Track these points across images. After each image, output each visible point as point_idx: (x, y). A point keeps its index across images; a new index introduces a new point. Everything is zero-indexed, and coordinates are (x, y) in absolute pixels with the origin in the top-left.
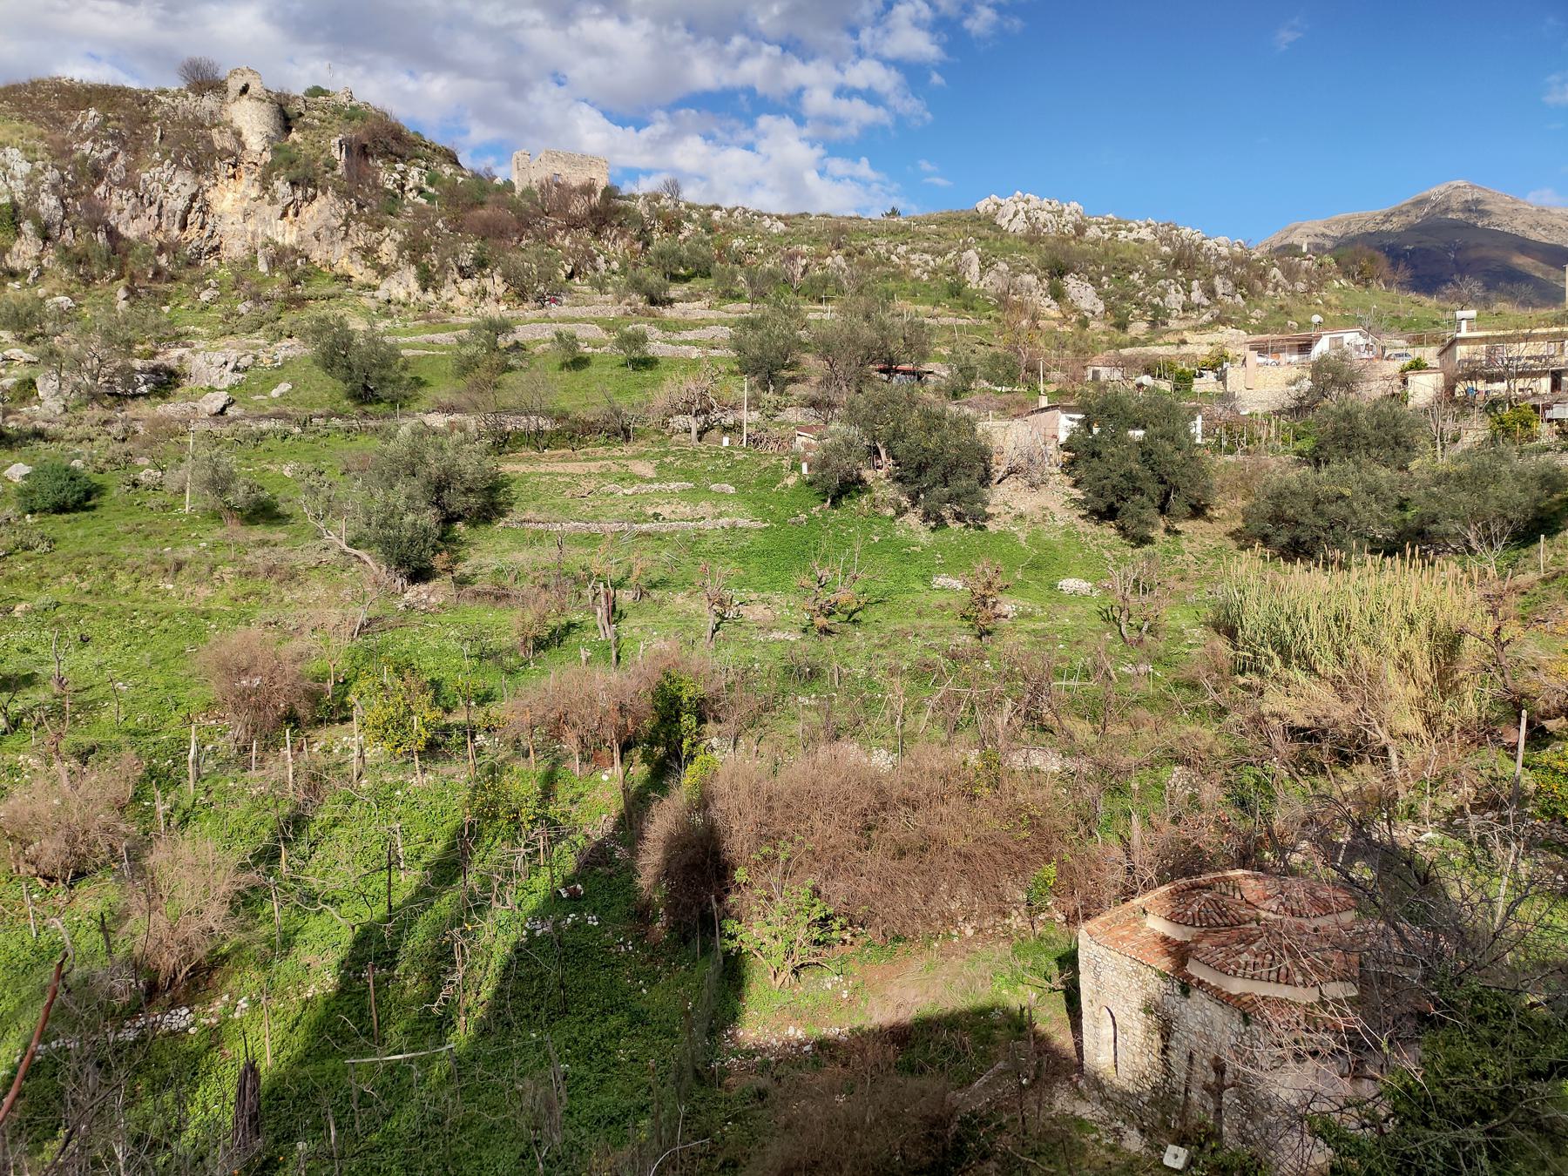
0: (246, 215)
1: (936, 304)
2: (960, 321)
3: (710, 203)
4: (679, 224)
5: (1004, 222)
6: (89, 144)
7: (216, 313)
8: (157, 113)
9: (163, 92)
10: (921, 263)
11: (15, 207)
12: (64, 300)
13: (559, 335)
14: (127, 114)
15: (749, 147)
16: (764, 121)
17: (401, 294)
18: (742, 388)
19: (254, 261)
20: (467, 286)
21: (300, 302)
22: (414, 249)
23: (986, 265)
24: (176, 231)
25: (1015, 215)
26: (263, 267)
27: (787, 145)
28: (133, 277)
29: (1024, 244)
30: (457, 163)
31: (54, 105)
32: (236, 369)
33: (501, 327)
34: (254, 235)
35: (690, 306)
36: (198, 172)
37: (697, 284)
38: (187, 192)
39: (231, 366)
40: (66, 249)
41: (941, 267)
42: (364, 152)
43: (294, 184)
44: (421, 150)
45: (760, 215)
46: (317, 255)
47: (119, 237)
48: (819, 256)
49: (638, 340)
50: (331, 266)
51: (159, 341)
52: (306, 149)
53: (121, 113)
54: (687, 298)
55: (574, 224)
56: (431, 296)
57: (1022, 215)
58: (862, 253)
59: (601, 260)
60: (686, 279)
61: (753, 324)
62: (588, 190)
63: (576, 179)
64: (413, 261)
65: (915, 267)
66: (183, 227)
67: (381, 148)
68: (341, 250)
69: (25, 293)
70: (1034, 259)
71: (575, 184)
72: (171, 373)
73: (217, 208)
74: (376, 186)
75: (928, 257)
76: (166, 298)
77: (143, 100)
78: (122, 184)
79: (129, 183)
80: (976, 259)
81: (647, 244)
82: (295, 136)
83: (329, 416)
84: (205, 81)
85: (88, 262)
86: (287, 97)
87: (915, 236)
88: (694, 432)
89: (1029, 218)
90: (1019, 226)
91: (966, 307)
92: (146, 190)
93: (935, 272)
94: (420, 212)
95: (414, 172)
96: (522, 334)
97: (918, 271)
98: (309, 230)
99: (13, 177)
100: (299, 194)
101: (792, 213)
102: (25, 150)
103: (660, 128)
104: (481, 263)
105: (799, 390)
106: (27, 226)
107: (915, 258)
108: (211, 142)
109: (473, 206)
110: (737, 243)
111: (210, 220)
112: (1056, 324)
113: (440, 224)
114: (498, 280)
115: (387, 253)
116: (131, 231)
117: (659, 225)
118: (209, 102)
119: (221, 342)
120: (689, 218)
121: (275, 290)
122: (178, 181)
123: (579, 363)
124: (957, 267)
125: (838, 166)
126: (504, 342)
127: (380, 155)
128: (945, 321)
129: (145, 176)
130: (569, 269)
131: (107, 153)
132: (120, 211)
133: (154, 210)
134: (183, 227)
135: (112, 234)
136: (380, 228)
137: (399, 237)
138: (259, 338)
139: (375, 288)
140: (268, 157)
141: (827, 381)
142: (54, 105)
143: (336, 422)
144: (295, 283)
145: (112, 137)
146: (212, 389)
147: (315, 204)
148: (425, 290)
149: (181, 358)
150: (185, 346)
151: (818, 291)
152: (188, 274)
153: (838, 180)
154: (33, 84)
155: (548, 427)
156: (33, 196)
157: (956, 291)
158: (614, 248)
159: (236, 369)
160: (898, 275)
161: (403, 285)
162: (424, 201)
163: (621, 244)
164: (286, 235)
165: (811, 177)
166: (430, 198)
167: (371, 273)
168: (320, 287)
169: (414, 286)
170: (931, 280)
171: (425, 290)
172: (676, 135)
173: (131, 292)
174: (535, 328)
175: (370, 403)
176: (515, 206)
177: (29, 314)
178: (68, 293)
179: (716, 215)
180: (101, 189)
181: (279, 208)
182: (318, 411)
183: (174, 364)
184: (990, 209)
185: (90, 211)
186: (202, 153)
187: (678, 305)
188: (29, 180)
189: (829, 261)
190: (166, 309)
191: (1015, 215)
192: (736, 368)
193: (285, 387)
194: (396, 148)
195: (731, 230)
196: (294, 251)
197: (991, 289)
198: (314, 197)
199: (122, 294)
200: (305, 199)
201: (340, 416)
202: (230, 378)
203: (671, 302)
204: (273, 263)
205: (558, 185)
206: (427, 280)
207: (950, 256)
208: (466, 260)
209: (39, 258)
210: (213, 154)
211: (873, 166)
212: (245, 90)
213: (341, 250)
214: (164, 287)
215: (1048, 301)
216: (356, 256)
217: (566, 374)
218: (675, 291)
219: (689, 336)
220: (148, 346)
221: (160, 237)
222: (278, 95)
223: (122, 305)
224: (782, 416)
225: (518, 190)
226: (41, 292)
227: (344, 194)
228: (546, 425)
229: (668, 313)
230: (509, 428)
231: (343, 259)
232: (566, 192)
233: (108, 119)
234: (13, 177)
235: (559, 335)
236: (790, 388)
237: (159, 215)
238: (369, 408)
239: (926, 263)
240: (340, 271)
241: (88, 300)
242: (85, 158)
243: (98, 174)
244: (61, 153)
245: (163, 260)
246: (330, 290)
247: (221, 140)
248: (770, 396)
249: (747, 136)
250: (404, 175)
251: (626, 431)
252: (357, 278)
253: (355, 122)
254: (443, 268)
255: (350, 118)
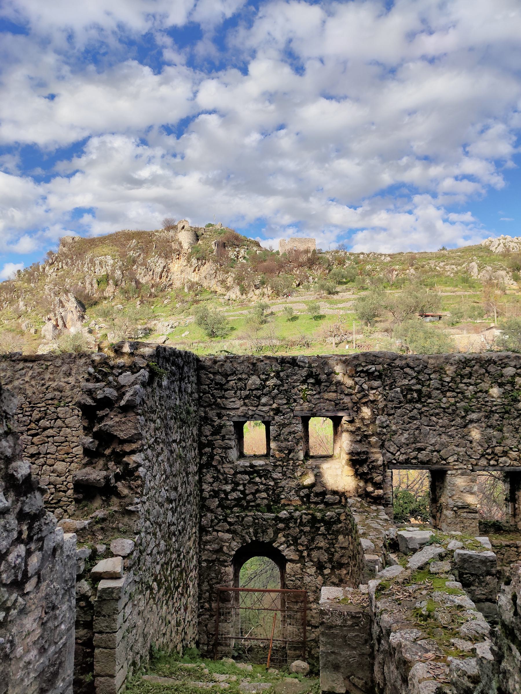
0: (182, 272)
1: (456, 286)
2: (466, 293)
3: (359, 252)
4: (344, 261)
5: (493, 249)
6: (132, 252)
7: (169, 307)
8: (154, 239)
9: (157, 231)
10: (450, 269)
11: (107, 275)
12: (120, 306)
13: (286, 308)
14: (145, 240)
15: (410, 212)
16: (417, 199)
17: (233, 296)
18: (355, 326)
19: (183, 288)
20: (257, 292)
21: (197, 302)
22: (239, 280)
23: (481, 268)
24: (158, 280)
25: (499, 245)
26: (186, 290)
27: (428, 210)
28: (142, 297)
29: (501, 257)
30: (259, 246)
31: (122, 240)
32: (172, 327)
33: (263, 307)
34: (184, 278)
35: (345, 294)
36: (166, 258)
37: (349, 285)
38: (162, 265)
39: (170, 326)
40: (122, 288)
41: (460, 270)
42: (224, 245)
43: (198, 259)
44: (245, 243)
45: (381, 255)
46: (205, 285)
47: (140, 283)
48: (403, 270)
49: (316, 308)
50: (210, 288)
51: (149, 319)
52: (203, 246)
53: (143, 240)
54: (344, 291)
55: (301, 265)
56: (244, 297)
57: (502, 245)
58: (423, 267)
59: (311, 278)
60: (345, 283)
61: (363, 299)
62: (307, 251)
63: (302, 247)
64: (238, 284)
65: (447, 271)
66: (161, 278)
67: (230, 243)
68: (213, 282)
69: (108, 305)
70: (505, 264)
71: (302, 249)
72: (151, 330)
73: (172, 270)
74: (228, 258)
75: (454, 267)
76: (152, 304)
77: (151, 235)
78: (142, 265)
79: (144, 264)
80: (476, 266)
81: (330, 271)
82: (200, 242)
83: (199, 342)
84: (170, 227)
85: (129, 293)
86: (198, 228)
87: (448, 258)
88: (334, 344)
89: (505, 246)
90: (501, 249)
91: (470, 287)
92: (149, 266)
93: (457, 273)
94: (243, 265)
95: (242, 251)
96: (274, 309)
97: (449, 273)
98: (203, 275)
99: (108, 265)
100: (200, 263)
101: (395, 252)
102: (112, 256)
103: (366, 207)
104: (263, 283)
105: (380, 326)
106: (111, 282)
107: (448, 268)
108: (171, 247)
109: (261, 262)
110: (368, 267)
111: (170, 275)
112: (515, 292)
113: (249, 270)
114: (269, 289)
115: (230, 281)
116: (143, 281)
117: (336, 263)
118: (171, 233)
119: (169, 318)
120: (349, 259)
121: (189, 298)
122: (159, 262)
123: (294, 319)
124: (467, 270)
125: (453, 216)
126: (265, 313)
127: (230, 246)
128: (458, 293)
129: (149, 261)
130: (298, 283)
131: (138, 254)
132: (140, 274)
133: (151, 273)
134: (161, 278)
135: (137, 282)
136: (228, 272)
137: (234, 276)
138: (182, 316)
139: (225, 295)
140: (190, 250)
141: (394, 322)
142: (122, 240)
143: (201, 344)
144: (196, 295)
145: (140, 249)
146: (163, 335)
147: (205, 266)
148: (242, 294)
149: (155, 324)
150: (157, 320)
151: (397, 285)
152: (161, 294)
153: (453, 223)
154: (117, 233)
155: (278, 344)
156: (113, 271)
157: (465, 280)
158: (317, 272)
159: (172, 327)
160: (439, 275)
161: (235, 293)
162: (245, 261)
163: (319, 271)
164: (195, 278)
165: (439, 224)
166: (247, 260)
167: (224, 289)
168: (206, 296)
169: (239, 293)
170: (455, 276)
171: (242, 294)
172: (373, 212)
173: (142, 302)
174: (278, 306)
175: (214, 337)
176: (278, 261)
177: (108, 312)
178: (122, 304)
179: (361, 256)
180: (135, 267)
181: (193, 268)
182: (195, 341)
183: (151, 327)
184: (487, 243)
185: (130, 274)
186: (168, 251)
187: (340, 294)
188: (113, 266)
189: (408, 271)
190: (152, 307)
191: (499, 245)
192: (357, 317)
193: (187, 333)
194: (236, 243)
195: (366, 262)
196: (197, 283)
197: (484, 279)
198: (205, 263)
199: (138, 303)
200: (202, 264)
201: (203, 342)
202: (169, 330)
203: (337, 293)
204: (190, 288)
205: (295, 251)
206: (243, 291)
207: (464, 265)
208: (257, 282)
209: (114, 292)
210: (172, 251)
211: (472, 215)
212: (183, 228)
213: (213, 282)
214: (152, 299)
215: (512, 281)
216: (219, 284)
217: (288, 323)
218: (339, 288)
219: (340, 306)
220: (145, 321)
221: (153, 282)
222: (195, 228)
223: (138, 307)
224: (373, 336)
225: (281, 254)
226: (113, 304)
227: (215, 261)
228: (278, 343)
229: (335, 297)
230: (263, 345)
231: (214, 285)
232: (298, 253)
233: (138, 243)
234: (108, 265)
235: (286, 308)
236: (377, 324)
237: (153, 274)
238: (213, 339)
239: (453, 269)
240: (213, 290)
241: (128, 306)
242: (131, 257)
243: (134, 262)
244: (123, 255)
245: (153, 290)
246: (208, 297)
247: (175, 246)
248: (369, 328)
249: (408, 207)
250: (238, 253)
251: (308, 344)
252: (219, 292)
253: (222, 235)
254: (249, 286)
255: (220, 234)
